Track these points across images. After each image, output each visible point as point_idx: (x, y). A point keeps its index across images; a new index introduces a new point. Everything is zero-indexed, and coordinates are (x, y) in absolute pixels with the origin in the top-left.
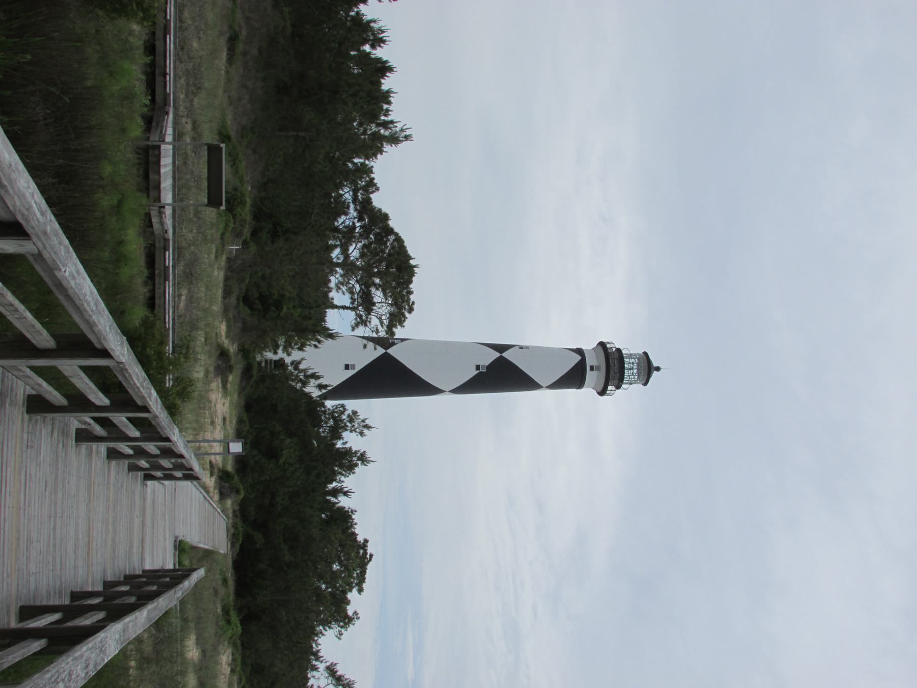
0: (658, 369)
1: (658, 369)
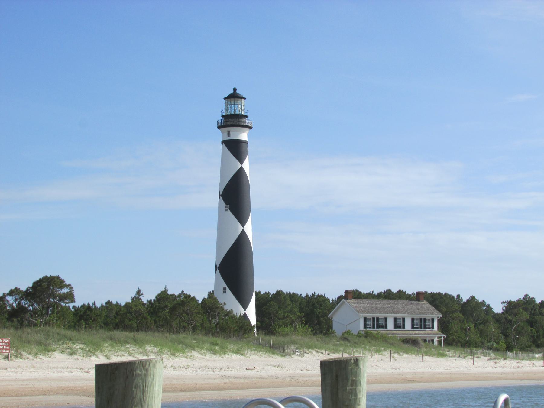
0: (235, 90)
1: (235, 90)
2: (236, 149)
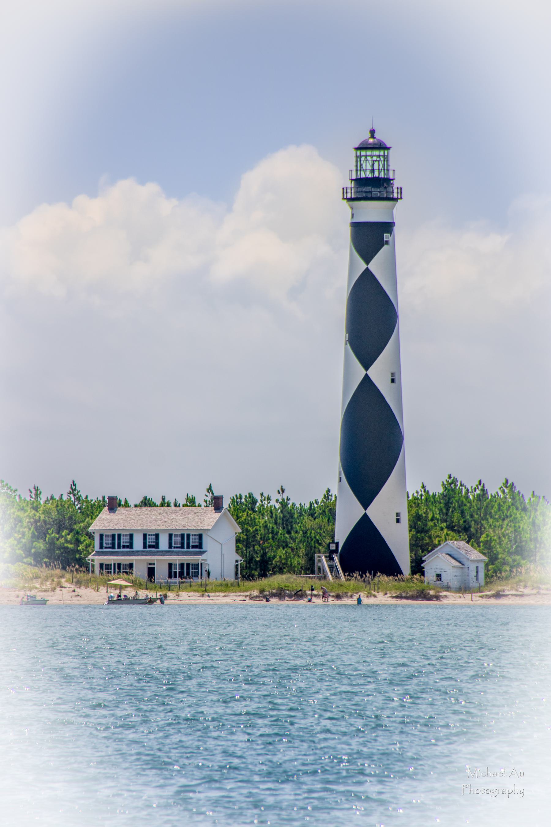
2: (370, 238)
